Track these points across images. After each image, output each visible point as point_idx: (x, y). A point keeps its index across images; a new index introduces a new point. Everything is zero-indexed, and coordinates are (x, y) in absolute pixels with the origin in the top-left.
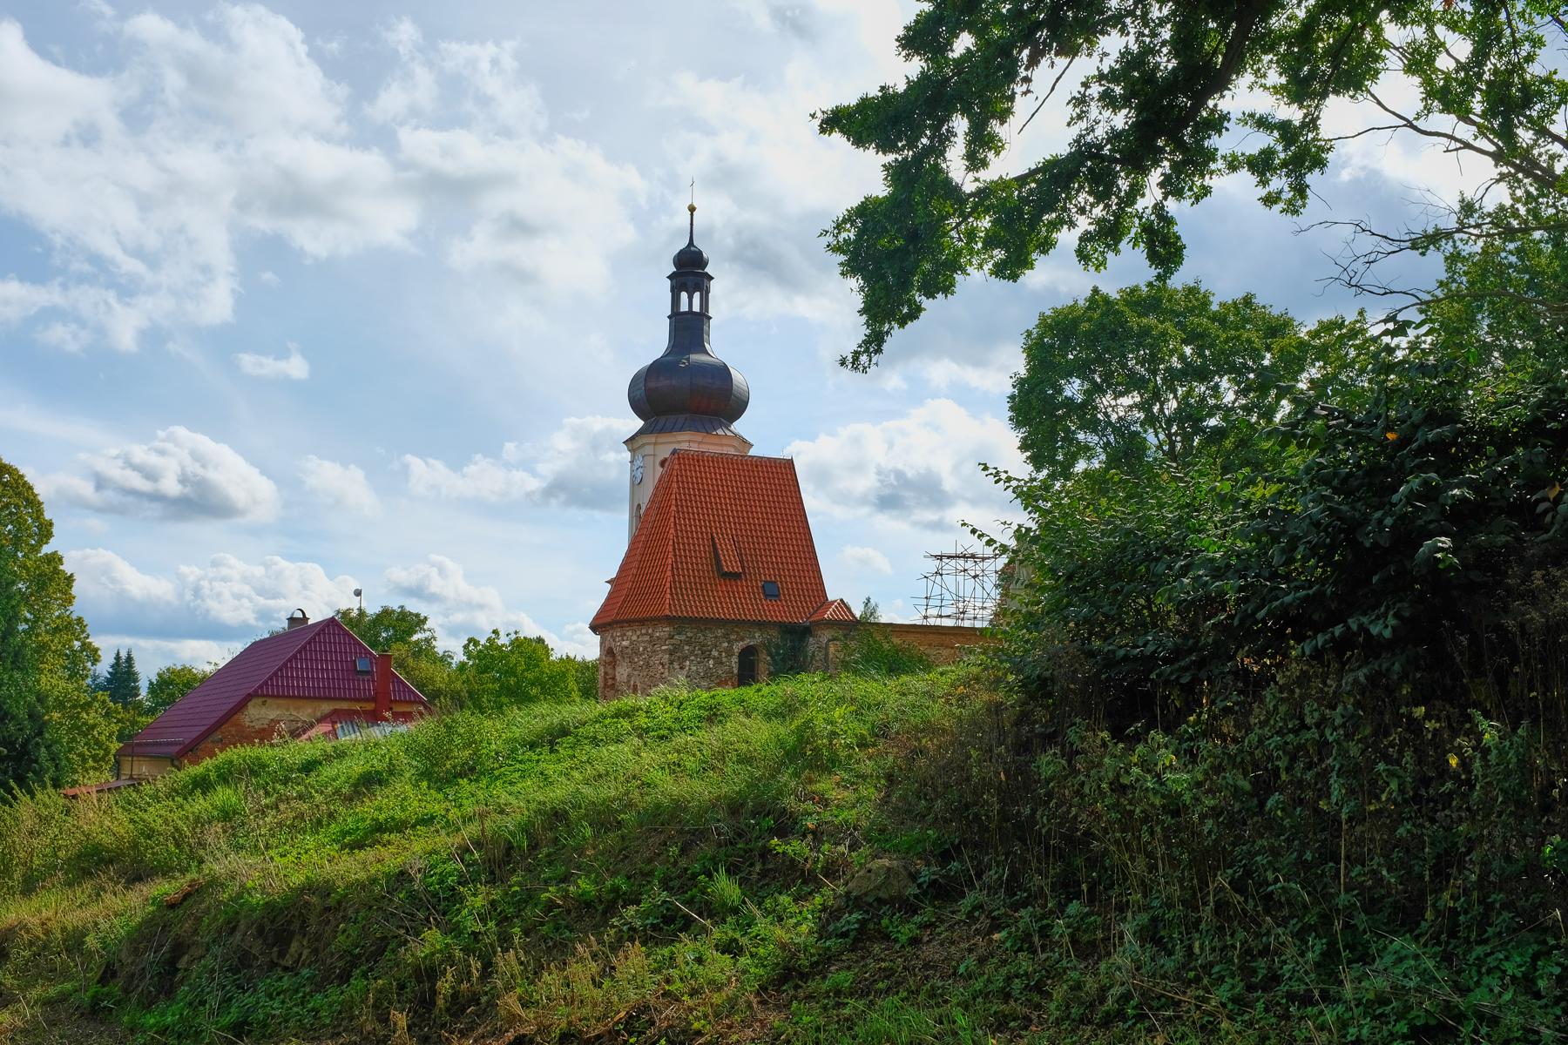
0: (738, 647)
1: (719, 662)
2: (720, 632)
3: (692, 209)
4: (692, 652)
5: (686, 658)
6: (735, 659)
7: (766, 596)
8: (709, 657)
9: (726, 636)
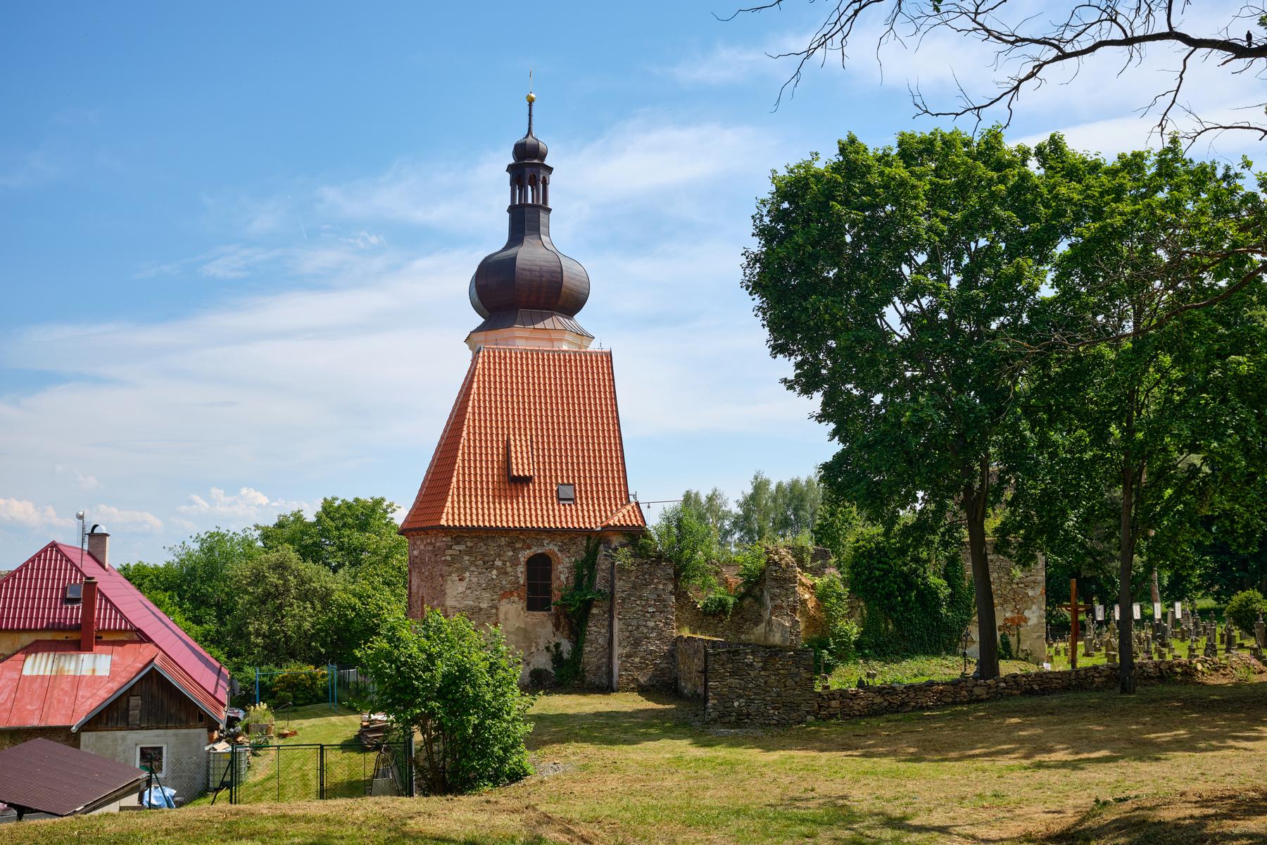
0: (524, 556)
1: (503, 572)
2: (503, 541)
3: (531, 101)
4: (472, 563)
5: (466, 569)
6: (521, 568)
7: (559, 499)
8: (493, 567)
9: (511, 545)
